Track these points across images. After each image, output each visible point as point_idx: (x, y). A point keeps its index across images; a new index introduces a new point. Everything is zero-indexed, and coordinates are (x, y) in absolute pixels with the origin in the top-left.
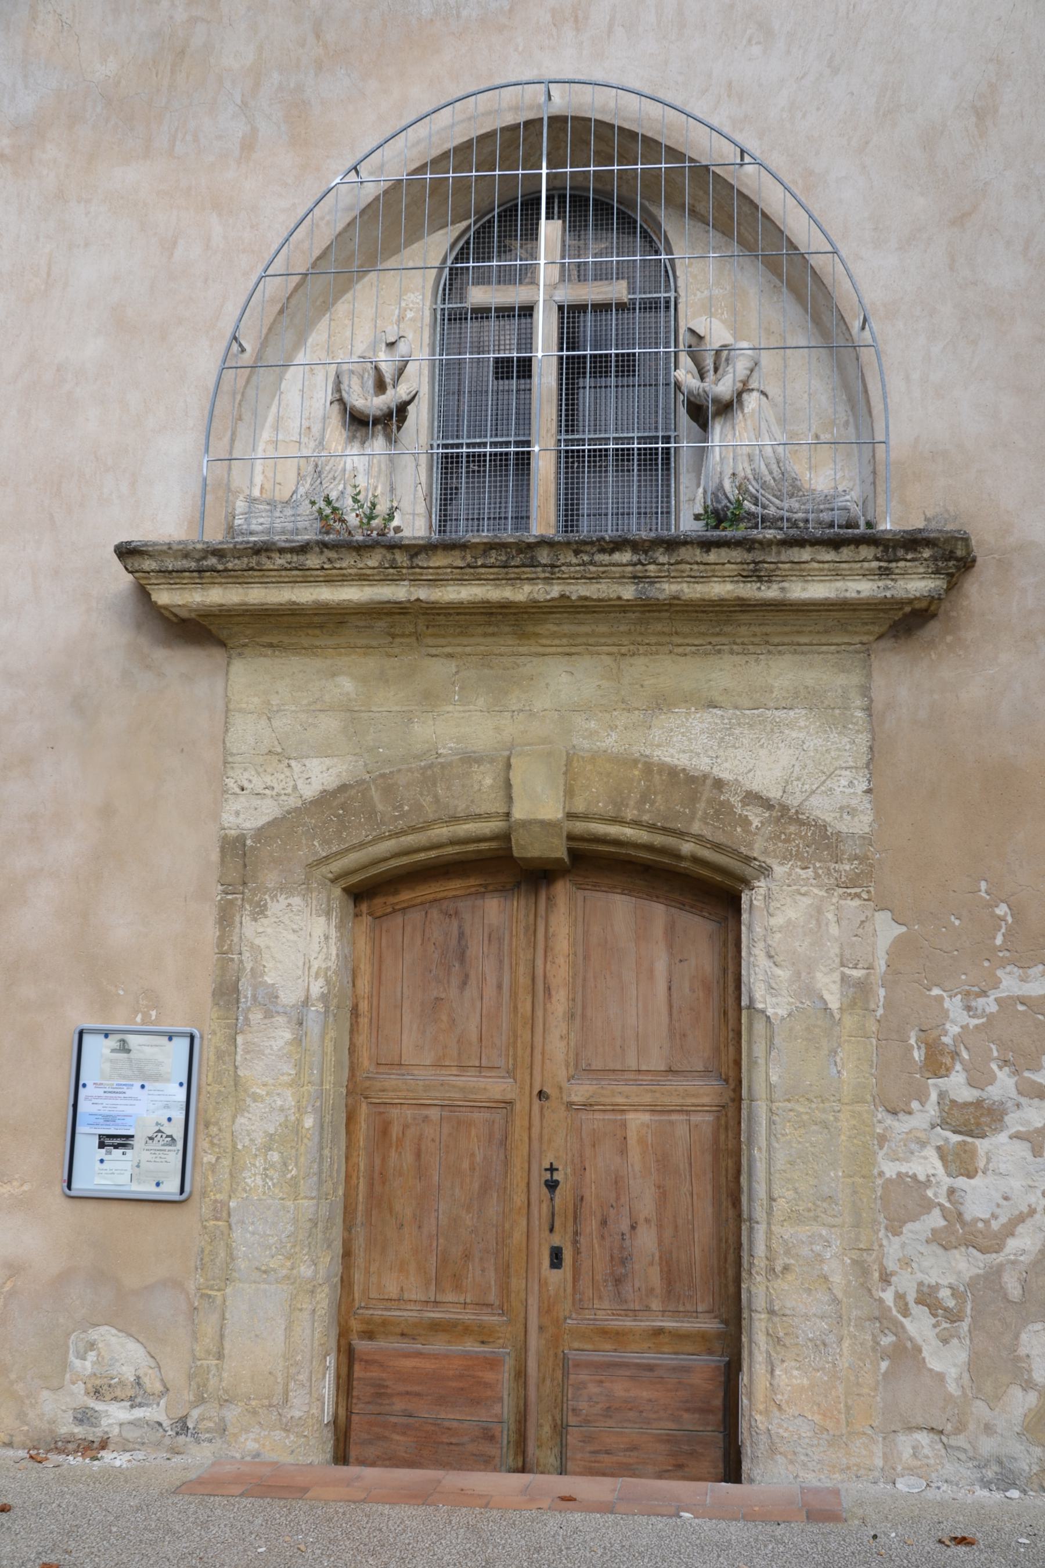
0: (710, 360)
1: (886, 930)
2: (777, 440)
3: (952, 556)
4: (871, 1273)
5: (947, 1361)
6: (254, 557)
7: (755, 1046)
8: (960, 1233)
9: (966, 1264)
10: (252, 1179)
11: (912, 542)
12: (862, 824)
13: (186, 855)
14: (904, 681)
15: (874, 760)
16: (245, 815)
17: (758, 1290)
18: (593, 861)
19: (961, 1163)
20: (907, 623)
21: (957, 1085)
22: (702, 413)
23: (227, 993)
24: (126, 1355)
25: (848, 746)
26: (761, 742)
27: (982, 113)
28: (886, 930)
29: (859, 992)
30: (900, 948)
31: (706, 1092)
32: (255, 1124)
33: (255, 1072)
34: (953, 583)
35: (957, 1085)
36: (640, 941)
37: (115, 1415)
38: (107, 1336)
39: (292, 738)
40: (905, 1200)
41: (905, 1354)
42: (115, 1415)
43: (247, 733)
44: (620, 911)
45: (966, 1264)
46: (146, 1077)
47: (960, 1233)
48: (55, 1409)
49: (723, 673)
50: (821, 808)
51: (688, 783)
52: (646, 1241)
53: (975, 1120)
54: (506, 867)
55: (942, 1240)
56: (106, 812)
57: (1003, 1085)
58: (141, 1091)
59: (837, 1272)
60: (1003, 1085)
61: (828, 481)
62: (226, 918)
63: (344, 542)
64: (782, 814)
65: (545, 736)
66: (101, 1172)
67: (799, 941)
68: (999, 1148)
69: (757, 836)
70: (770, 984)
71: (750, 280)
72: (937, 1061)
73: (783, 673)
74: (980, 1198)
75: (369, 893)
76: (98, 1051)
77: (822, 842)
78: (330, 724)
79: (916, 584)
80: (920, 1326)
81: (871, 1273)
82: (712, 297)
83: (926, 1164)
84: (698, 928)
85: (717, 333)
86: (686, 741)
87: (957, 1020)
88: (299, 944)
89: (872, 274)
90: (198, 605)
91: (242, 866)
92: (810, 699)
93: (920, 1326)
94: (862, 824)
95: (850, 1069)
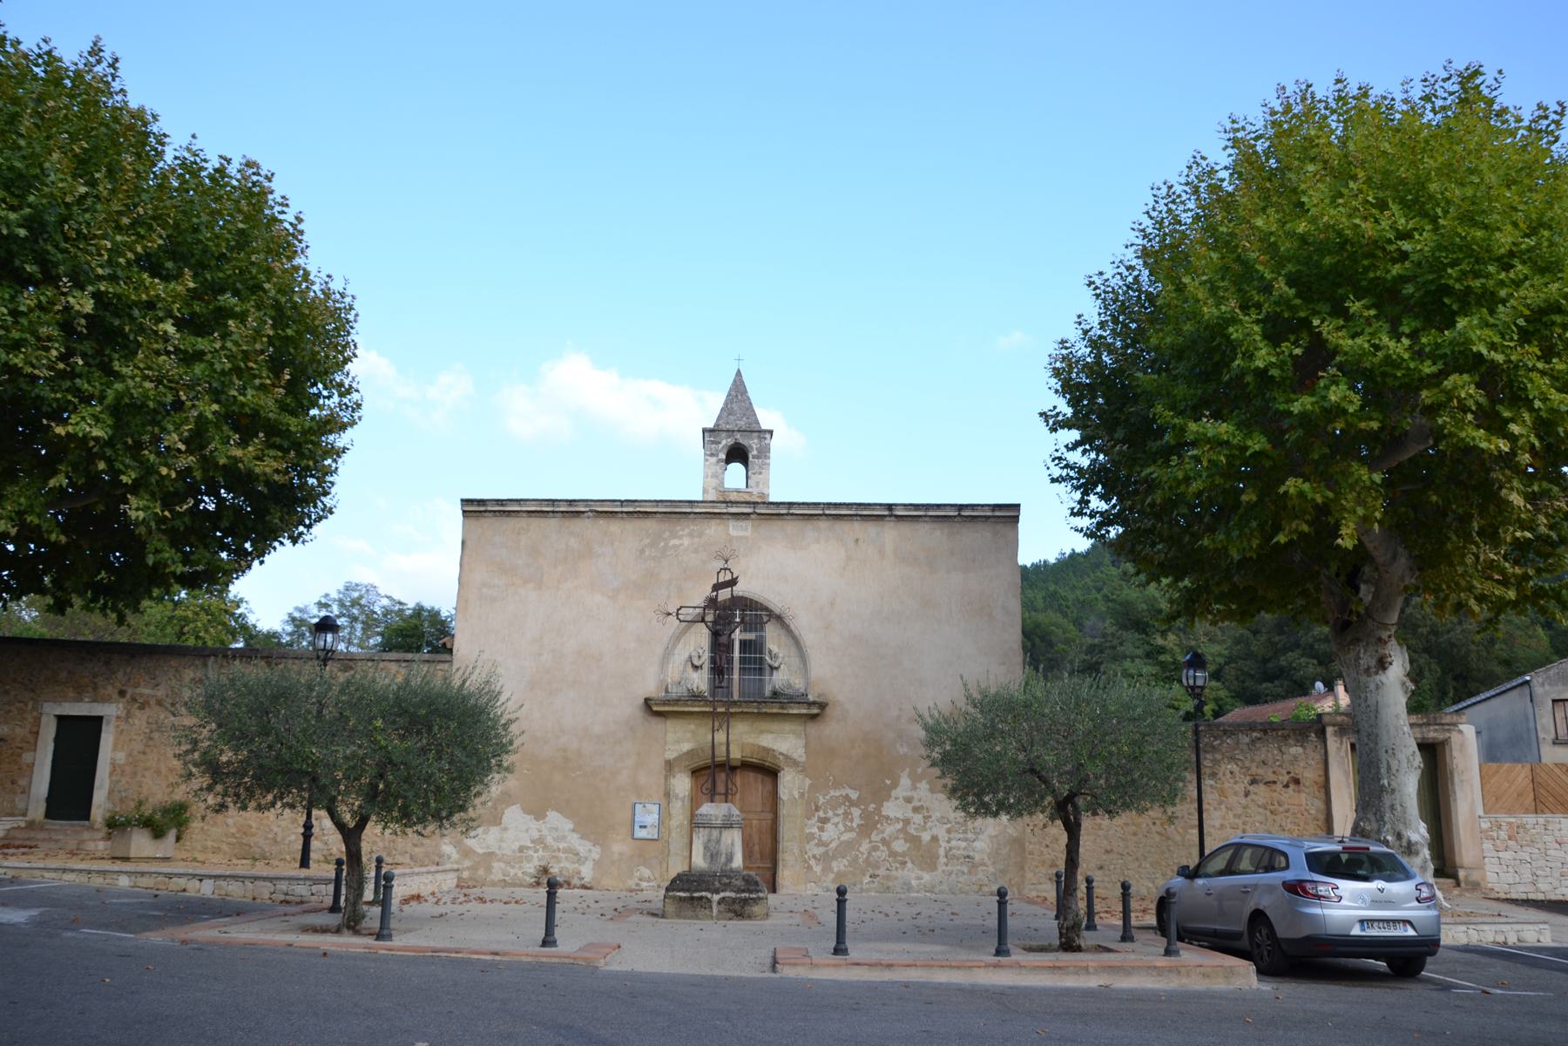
0: (774, 657)
1: (808, 782)
2: (784, 677)
3: (823, 706)
4: (803, 852)
5: (818, 869)
6: (677, 701)
7: (781, 806)
8: (821, 843)
9: (822, 849)
10: (673, 834)
11: (814, 703)
12: (803, 759)
13: (657, 764)
14: (813, 729)
15: (806, 746)
16: (670, 755)
17: (780, 856)
18: (746, 766)
19: (822, 829)
20: (813, 717)
21: (821, 814)
22: (772, 668)
23: (667, 795)
24: (646, 872)
25: (802, 742)
26: (783, 741)
27: (832, 604)
28: (808, 782)
29: (802, 795)
30: (811, 786)
31: (769, 816)
32: (674, 823)
33: (673, 812)
34: (693, 815)
35: (821, 814)
36: (754, 787)
37: (644, 884)
38: (642, 868)
39: (682, 739)
40: (811, 837)
41: (809, 868)
42: (644, 884)
43: (670, 737)
44: (751, 776)
45: (822, 849)
46: (650, 813)
47: (821, 843)
48: (631, 883)
49: (775, 726)
50: (795, 756)
51: (767, 750)
52: (756, 848)
53: (825, 821)
54: (729, 768)
55: (817, 845)
56: (639, 754)
57: (830, 814)
58: (648, 816)
59: (796, 851)
60: (830, 814)
61: (798, 684)
62: (666, 778)
63: (695, 697)
64: (787, 757)
65: (744, 738)
66: (640, 833)
67: (790, 784)
68: (829, 826)
69: (781, 761)
70: (783, 793)
71: (784, 639)
72: (817, 809)
73: (787, 726)
74: (825, 836)
75: (695, 772)
76: (638, 807)
77: (795, 763)
78: (689, 735)
79: (815, 711)
80: (812, 862)
81: (803, 852)
82: (773, 640)
83: (815, 830)
84: (768, 780)
85: (775, 649)
86: (767, 741)
87: (821, 801)
88: (682, 784)
89: (809, 638)
90: (654, 709)
91: (670, 766)
92: (794, 732)
93: (812, 862)
94: (803, 759)
95: (800, 811)
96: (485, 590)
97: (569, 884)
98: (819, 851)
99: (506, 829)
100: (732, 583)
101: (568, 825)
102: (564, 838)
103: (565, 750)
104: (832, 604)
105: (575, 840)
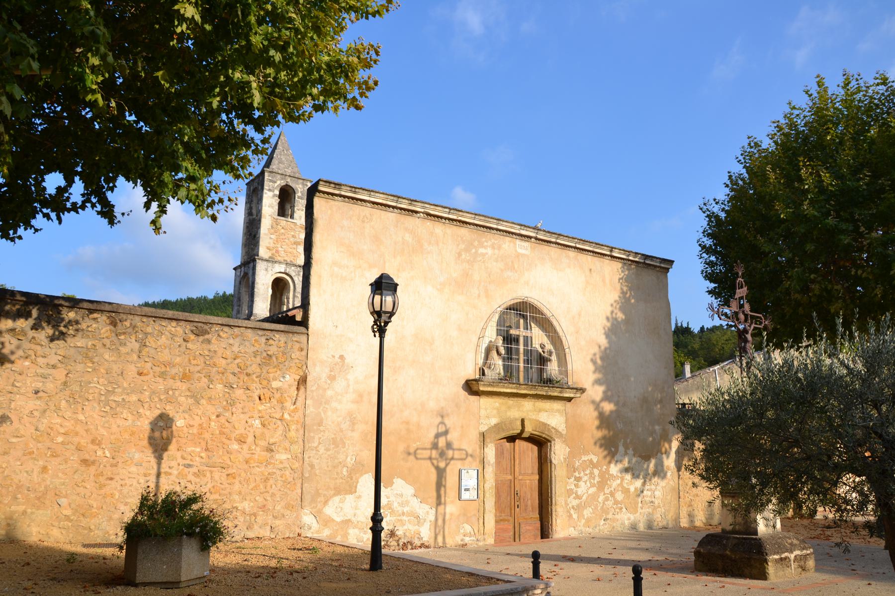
15: (567, 421)
19: (577, 486)
35: (577, 474)
47: (578, 497)
50: (560, 429)
52: (529, 502)
80: (572, 512)
83: (573, 487)
93: (572, 512)
96: (336, 269)
97: (411, 544)
98: (575, 502)
99: (360, 497)
100: (446, 433)
101: (409, 490)
102: (407, 503)
103: (407, 423)
104: (580, 315)
105: (415, 503)
